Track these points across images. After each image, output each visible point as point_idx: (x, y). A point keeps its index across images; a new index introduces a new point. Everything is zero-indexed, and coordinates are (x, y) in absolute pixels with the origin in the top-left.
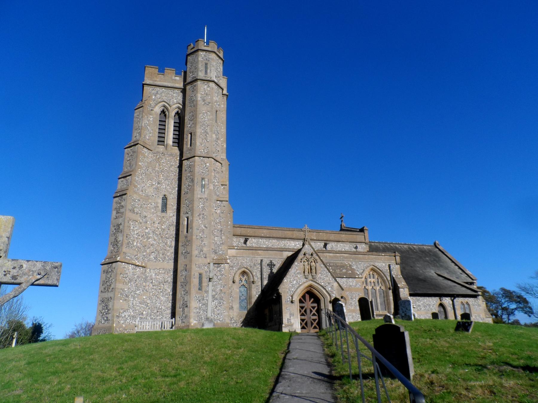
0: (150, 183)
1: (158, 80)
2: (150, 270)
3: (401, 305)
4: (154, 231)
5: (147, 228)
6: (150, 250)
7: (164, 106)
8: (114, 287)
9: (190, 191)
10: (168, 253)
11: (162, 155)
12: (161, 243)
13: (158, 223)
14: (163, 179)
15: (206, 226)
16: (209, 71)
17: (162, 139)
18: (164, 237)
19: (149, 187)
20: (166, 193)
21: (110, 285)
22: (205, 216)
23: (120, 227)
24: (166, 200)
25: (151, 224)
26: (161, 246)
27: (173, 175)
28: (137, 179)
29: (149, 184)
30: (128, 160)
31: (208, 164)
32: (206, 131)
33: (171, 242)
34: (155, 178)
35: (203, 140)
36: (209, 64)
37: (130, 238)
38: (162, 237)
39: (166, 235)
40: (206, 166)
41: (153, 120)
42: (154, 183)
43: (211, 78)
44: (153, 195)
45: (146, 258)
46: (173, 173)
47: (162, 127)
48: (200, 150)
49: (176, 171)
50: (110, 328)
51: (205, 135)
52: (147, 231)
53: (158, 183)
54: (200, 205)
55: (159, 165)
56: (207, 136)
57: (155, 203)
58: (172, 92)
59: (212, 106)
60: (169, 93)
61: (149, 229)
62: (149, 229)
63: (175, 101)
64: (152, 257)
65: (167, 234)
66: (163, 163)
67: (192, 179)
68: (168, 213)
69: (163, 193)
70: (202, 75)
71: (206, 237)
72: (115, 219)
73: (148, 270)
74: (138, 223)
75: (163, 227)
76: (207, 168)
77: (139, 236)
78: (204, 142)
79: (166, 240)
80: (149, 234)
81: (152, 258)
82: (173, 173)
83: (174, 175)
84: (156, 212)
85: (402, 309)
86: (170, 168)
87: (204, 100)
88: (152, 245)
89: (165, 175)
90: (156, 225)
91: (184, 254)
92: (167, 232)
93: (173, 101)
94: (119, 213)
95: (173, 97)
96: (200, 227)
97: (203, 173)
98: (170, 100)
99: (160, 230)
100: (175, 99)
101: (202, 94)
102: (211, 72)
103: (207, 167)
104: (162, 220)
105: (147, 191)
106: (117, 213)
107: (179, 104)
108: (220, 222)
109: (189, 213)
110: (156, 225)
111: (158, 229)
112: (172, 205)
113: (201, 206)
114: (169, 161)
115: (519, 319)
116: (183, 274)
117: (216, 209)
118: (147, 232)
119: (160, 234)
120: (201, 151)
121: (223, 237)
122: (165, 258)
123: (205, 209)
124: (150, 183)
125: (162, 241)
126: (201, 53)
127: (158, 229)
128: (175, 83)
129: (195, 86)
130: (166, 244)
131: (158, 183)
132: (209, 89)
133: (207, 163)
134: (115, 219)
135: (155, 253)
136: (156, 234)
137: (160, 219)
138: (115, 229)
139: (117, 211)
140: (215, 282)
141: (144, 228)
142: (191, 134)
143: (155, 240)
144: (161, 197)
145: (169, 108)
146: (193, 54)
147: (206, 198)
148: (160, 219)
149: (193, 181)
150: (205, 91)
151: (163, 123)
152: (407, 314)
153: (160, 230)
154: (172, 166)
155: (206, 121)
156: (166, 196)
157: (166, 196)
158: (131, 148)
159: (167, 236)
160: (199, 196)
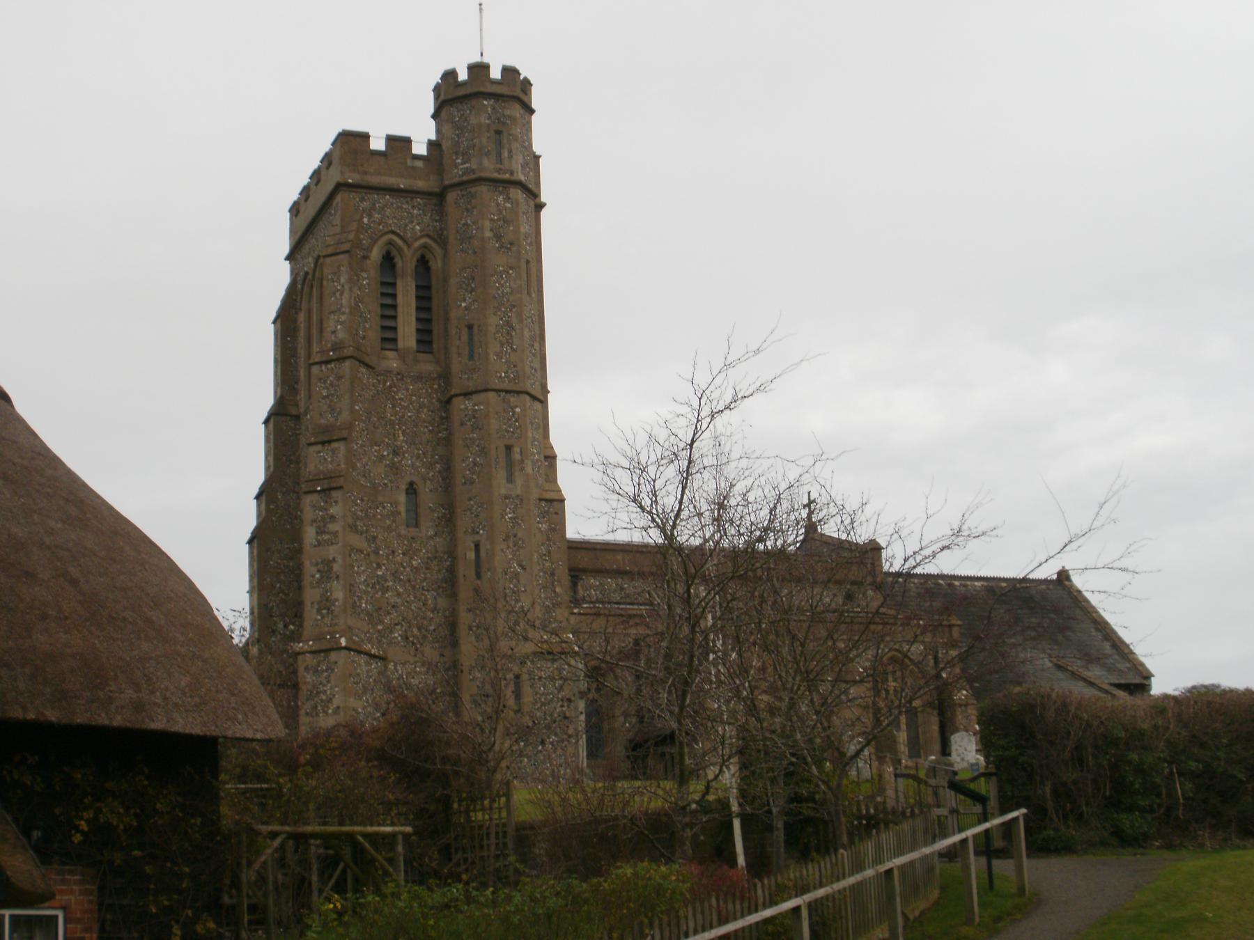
0: (376, 454)
1: (372, 171)
2: (395, 666)
3: (956, 742)
4: (396, 572)
5: (379, 566)
6: (391, 619)
7: (391, 243)
8: (341, 705)
9: (478, 477)
10: (431, 625)
11: (397, 379)
12: (413, 602)
13: (404, 554)
14: (406, 442)
15: (524, 563)
16: (506, 154)
17: (389, 335)
18: (418, 586)
19: (374, 462)
20: (415, 479)
21: (330, 700)
22: (520, 539)
23: (332, 567)
24: (414, 496)
25: (388, 556)
26: (413, 608)
27: (426, 430)
28: (355, 447)
29: (375, 456)
30: (324, 398)
31: (518, 410)
32: (508, 322)
33: (435, 598)
34: (387, 440)
35: (502, 345)
36: (505, 134)
37: (355, 592)
38: (414, 587)
39: (422, 582)
40: (513, 415)
41: (368, 284)
42: (385, 453)
43: (512, 173)
44: (385, 484)
45: (384, 637)
46: (427, 427)
47: (389, 301)
48: (496, 372)
49: (434, 419)
50: (957, 730)
51: (508, 333)
52: (380, 573)
53: (396, 453)
54: (506, 514)
55: (394, 406)
56: (511, 336)
57: (391, 504)
58: (407, 202)
59: (519, 252)
60: (401, 208)
61: (384, 568)
62: (384, 568)
63: (418, 227)
64: (396, 635)
65: (425, 579)
66: (401, 399)
67: (484, 448)
68: (423, 529)
69: (408, 479)
70: (492, 167)
71: (526, 591)
72: (315, 546)
73: (391, 666)
74: (365, 555)
75: (414, 563)
76: (516, 421)
77: (368, 585)
78: (506, 352)
79: (423, 594)
80: (386, 580)
81: (397, 638)
82: (427, 427)
83: (429, 431)
84: (397, 527)
85: (957, 750)
86: (418, 412)
87: (498, 237)
88: (393, 607)
89: (408, 431)
90: (399, 559)
91: (474, 629)
92: (425, 574)
93: (413, 229)
94: (324, 532)
95: (412, 217)
96: (511, 567)
97: (508, 432)
98: (406, 225)
99: (408, 569)
100: (418, 224)
101: (492, 220)
102: (510, 157)
103: (516, 416)
104: (411, 545)
105: (372, 475)
106: (320, 532)
107: (428, 236)
108: (549, 552)
109: (481, 532)
110: (399, 559)
111: (404, 568)
112: (430, 507)
113: (510, 516)
114: (415, 395)
115: (518, 67)
116: (478, 675)
117: (538, 522)
118: (382, 577)
119: (409, 580)
120: (500, 377)
121: (558, 590)
122: (424, 637)
123: (519, 525)
124: (376, 454)
125: (415, 597)
126: (485, 102)
127: (404, 568)
128: (415, 179)
129: (473, 196)
130: (424, 604)
131: (396, 453)
132: (509, 205)
133: (517, 407)
134: (315, 546)
135: (402, 626)
136: (400, 580)
137: (406, 542)
138: (319, 571)
139: (319, 527)
140: (551, 694)
141: (375, 565)
142: (470, 327)
143: (399, 595)
144: (404, 487)
145: (405, 248)
146: (461, 103)
147: (518, 496)
148: (406, 542)
149: (483, 451)
150: (500, 210)
151: (390, 291)
152: (966, 759)
153: (408, 569)
154: (422, 406)
155: (507, 294)
156: (415, 486)
157: (415, 486)
158: (329, 366)
159: (425, 584)
160: (503, 492)
